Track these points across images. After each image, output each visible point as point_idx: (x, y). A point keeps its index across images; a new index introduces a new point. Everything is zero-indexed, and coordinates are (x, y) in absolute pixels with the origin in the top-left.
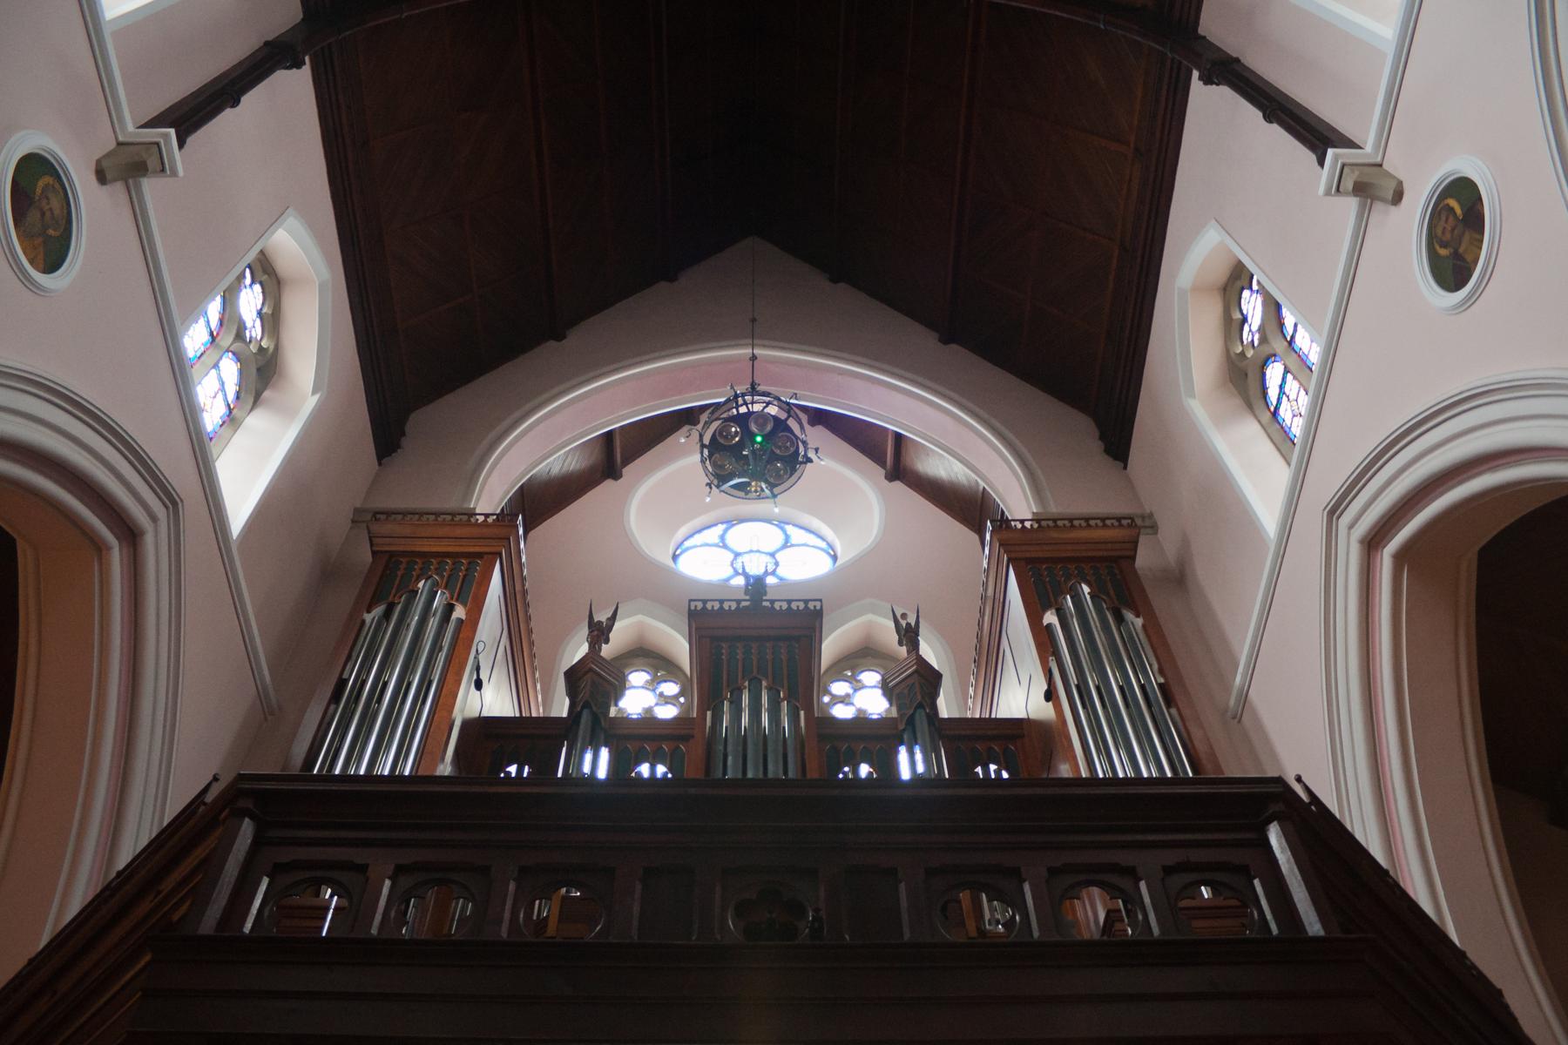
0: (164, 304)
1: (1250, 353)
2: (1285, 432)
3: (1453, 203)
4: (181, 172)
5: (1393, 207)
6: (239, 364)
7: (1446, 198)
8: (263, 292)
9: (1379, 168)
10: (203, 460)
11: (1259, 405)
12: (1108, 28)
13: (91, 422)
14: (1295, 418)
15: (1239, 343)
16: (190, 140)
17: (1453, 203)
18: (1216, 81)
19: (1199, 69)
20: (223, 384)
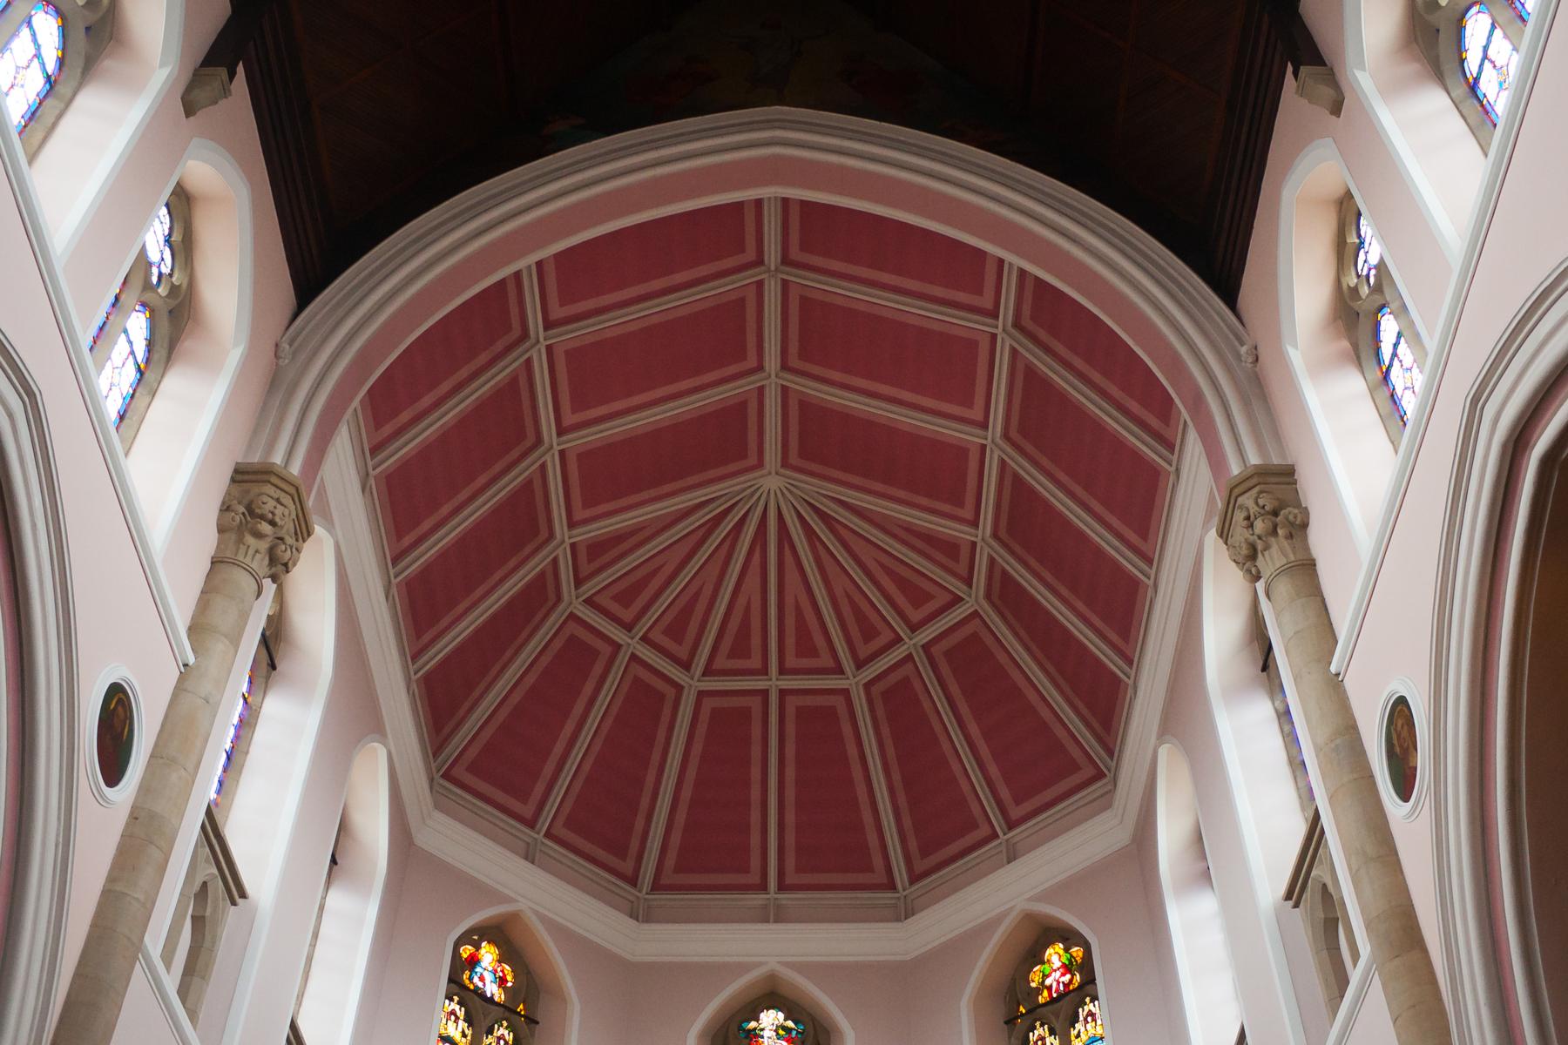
1: (1364, 291)
2: (1486, 110)
6: (60, 20)
8: (169, 213)
11: (1367, 353)
13: (48, 506)
14: (1406, 391)
15: (1353, 269)
20: (38, 47)
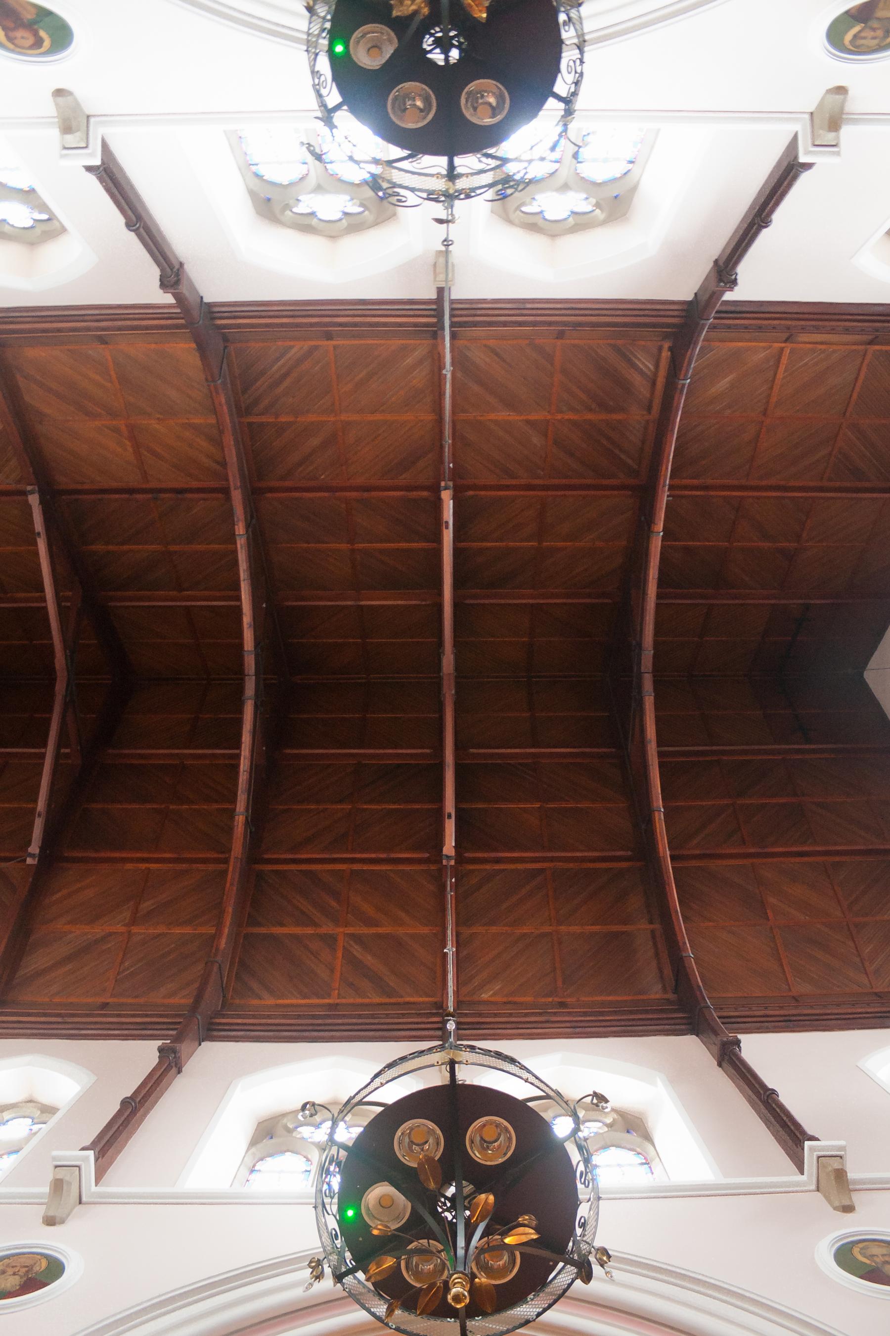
0: (129, 1197)
3: (849, 37)
4: (842, 1143)
5: (850, 92)
7: (844, 44)
9: (815, 115)
10: (152, 1198)
12: (689, 376)
16: (810, 1131)
17: (849, 37)
18: (733, 277)
19: (722, 293)
